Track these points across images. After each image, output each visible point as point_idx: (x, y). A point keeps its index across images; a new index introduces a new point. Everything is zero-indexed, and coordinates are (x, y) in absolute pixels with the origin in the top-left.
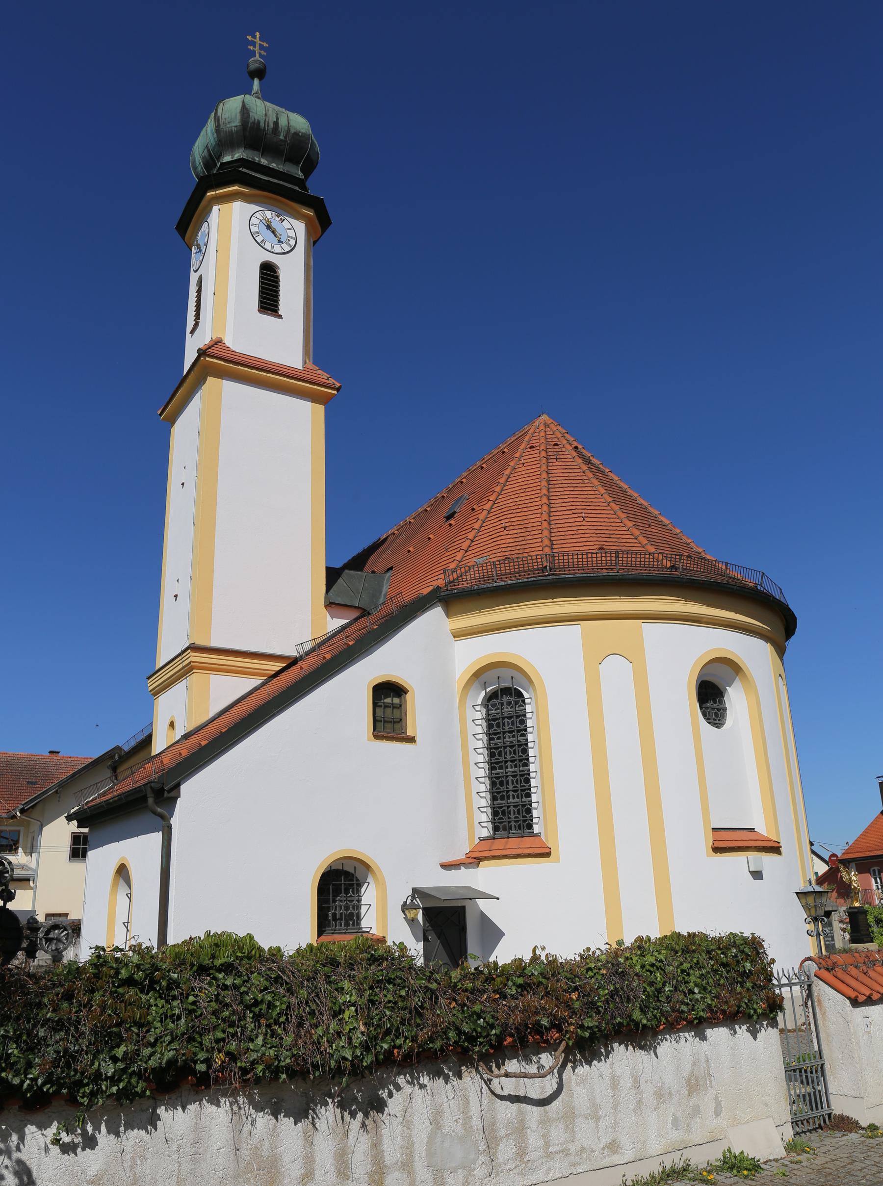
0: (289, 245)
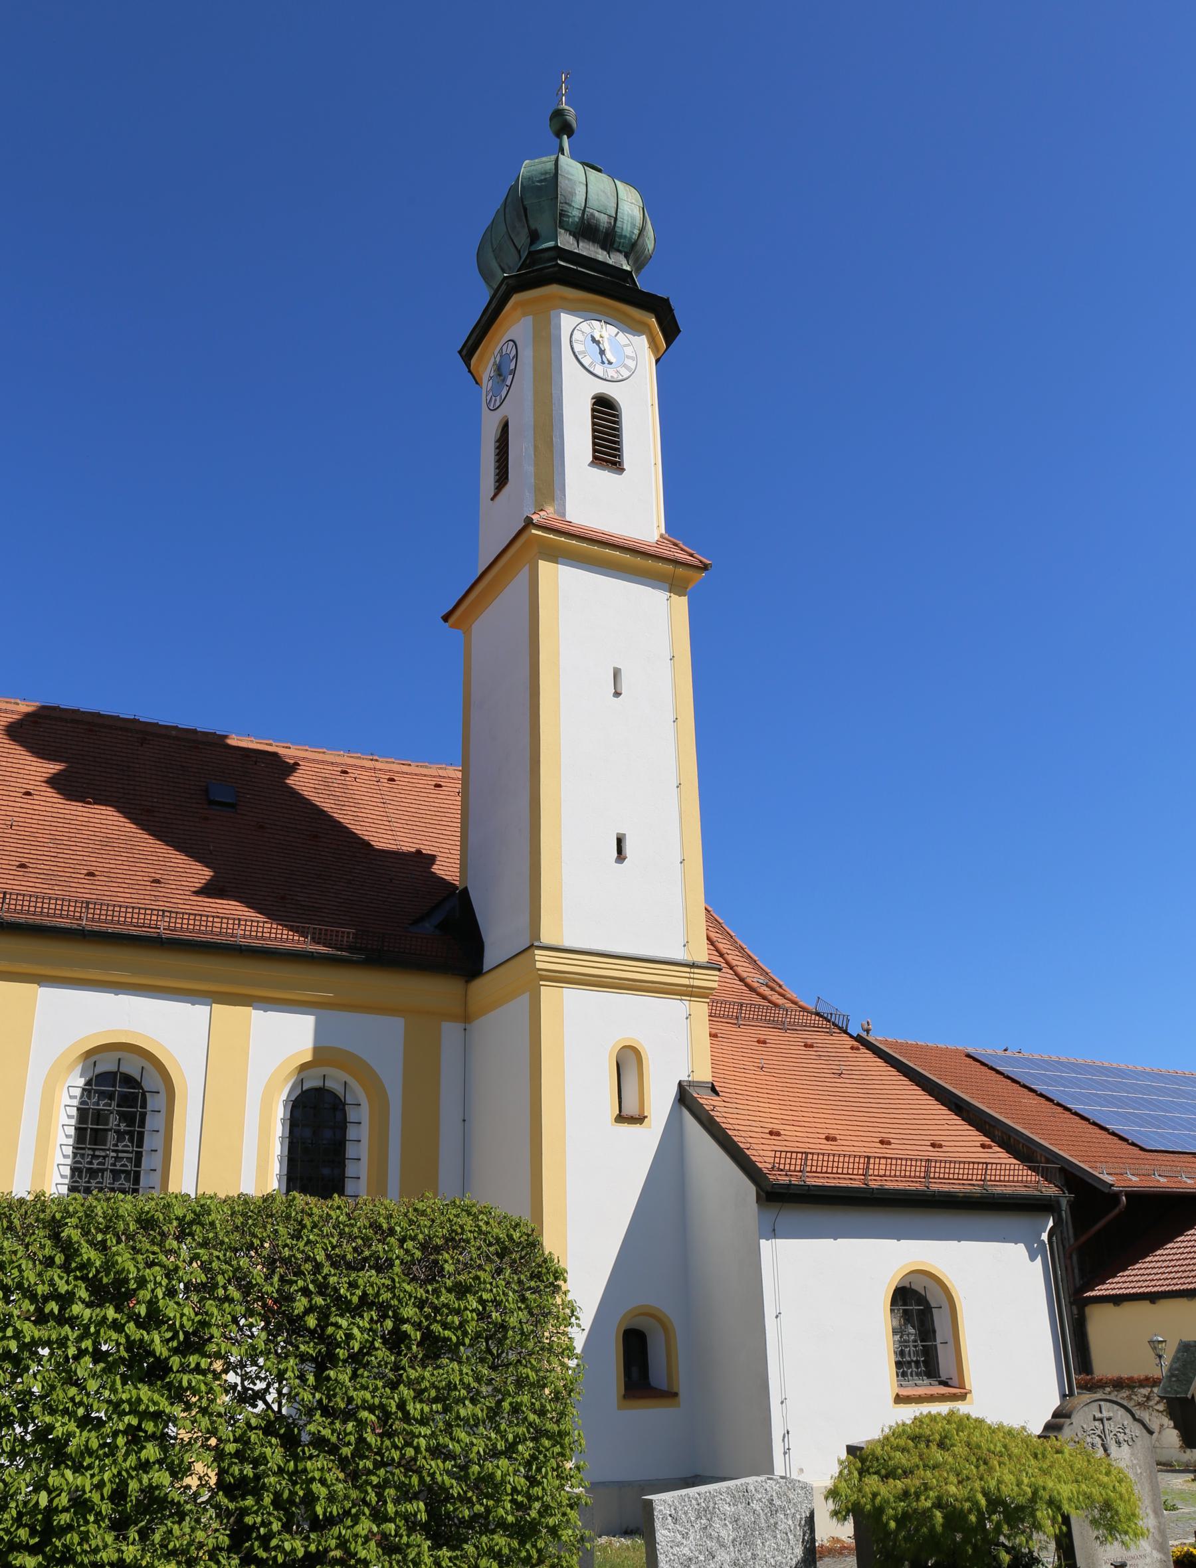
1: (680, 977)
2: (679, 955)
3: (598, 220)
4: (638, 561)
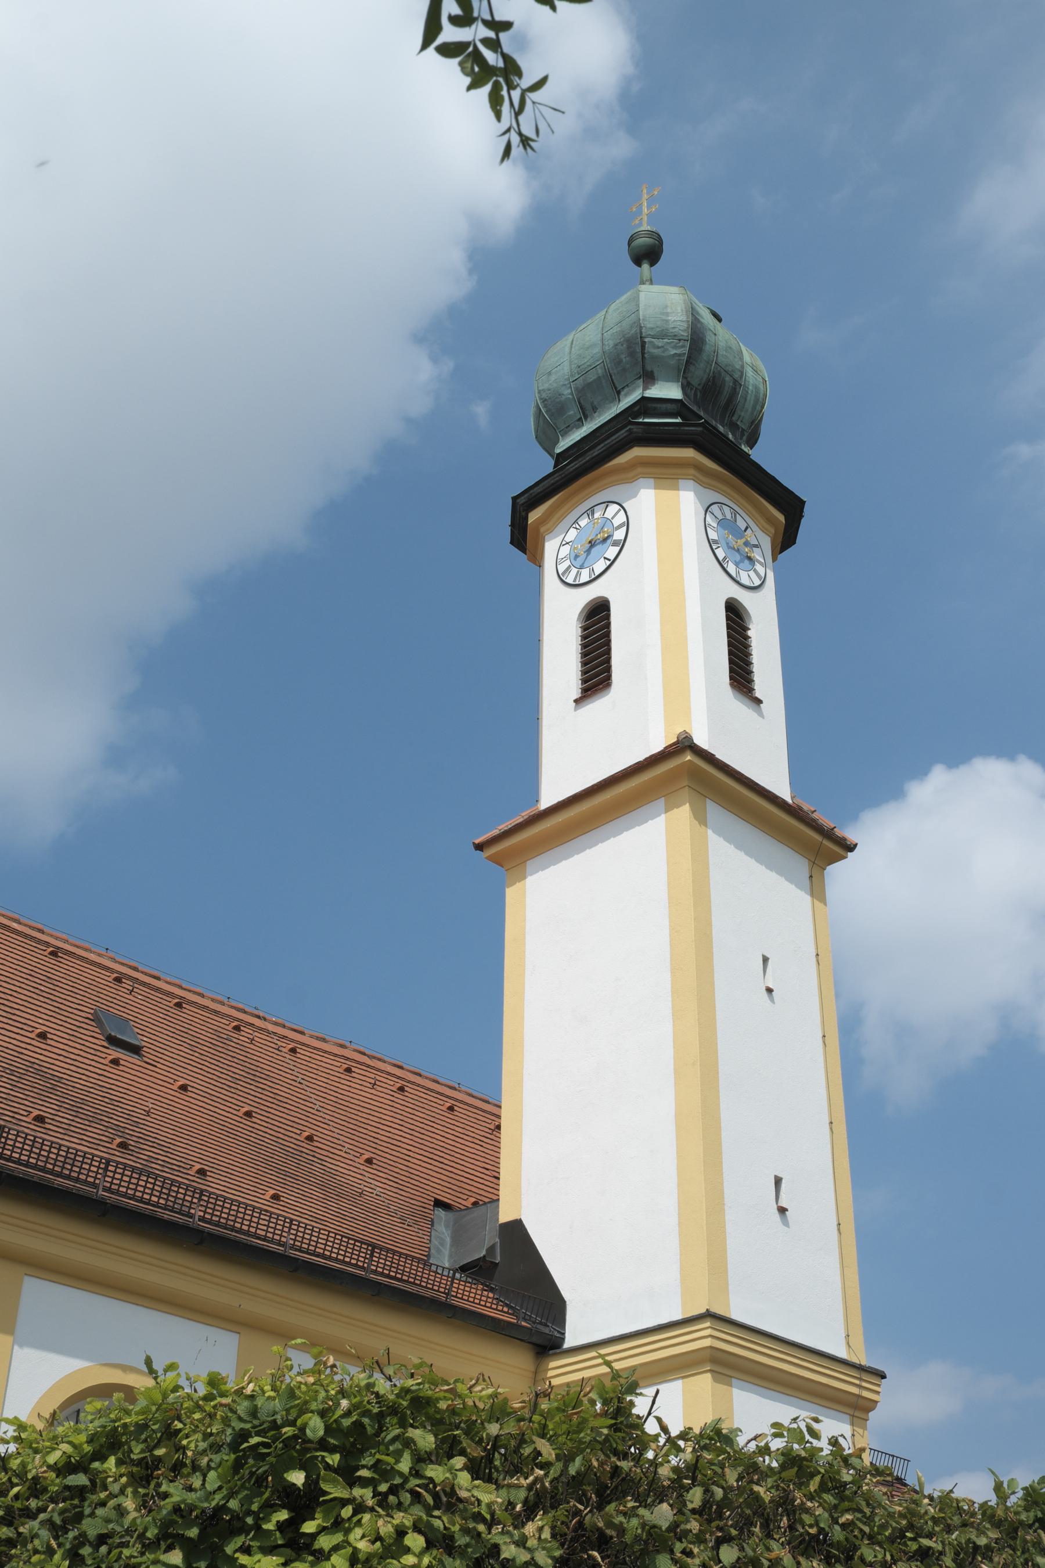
2: (842, 1353)
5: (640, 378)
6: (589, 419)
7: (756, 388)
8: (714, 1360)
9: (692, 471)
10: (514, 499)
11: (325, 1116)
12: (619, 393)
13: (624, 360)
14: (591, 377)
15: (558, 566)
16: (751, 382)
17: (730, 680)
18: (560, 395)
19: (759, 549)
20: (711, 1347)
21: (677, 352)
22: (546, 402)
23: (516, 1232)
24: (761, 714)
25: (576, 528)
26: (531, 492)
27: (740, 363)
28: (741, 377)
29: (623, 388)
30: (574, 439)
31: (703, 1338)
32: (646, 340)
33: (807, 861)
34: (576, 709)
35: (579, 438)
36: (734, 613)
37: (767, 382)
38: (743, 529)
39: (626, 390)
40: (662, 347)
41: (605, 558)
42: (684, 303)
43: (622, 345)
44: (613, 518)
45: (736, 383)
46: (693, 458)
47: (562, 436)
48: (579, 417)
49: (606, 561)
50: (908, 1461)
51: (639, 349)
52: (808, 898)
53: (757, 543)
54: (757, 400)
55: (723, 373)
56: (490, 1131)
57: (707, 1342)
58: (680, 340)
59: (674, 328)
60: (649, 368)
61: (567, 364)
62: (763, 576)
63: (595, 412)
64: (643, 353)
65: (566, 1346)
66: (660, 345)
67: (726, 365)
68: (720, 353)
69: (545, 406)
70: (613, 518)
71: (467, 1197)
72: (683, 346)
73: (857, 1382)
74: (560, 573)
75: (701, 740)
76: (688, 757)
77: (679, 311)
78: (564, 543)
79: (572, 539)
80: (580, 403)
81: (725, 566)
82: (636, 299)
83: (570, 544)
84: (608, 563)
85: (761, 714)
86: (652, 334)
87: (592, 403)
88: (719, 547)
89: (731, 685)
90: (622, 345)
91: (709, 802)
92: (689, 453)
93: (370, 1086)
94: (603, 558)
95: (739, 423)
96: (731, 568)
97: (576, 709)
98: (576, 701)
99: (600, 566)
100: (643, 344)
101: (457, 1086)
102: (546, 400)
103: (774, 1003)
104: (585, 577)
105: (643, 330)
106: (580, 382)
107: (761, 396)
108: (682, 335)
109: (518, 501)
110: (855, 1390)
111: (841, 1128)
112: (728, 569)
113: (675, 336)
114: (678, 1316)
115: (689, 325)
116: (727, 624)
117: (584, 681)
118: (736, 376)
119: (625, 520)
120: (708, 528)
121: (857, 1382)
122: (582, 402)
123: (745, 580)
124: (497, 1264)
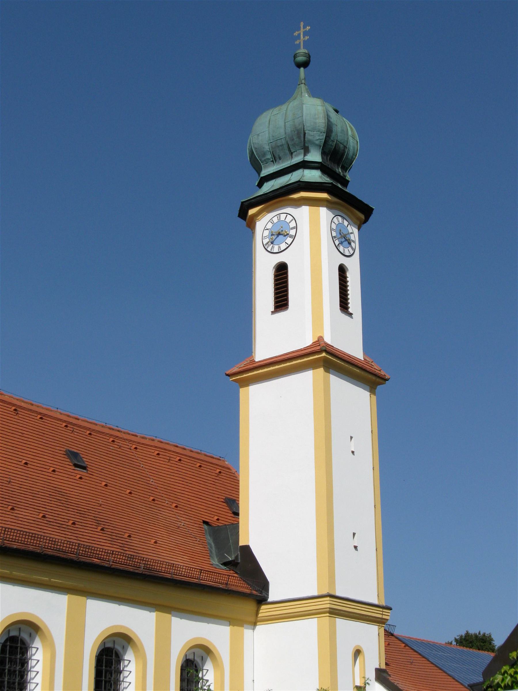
0: (291, 236)
1: (377, 613)
2: (376, 602)
3: (340, 148)
4: (363, 373)
5: (302, 149)
6: (277, 162)
7: (354, 148)
8: (330, 613)
9: (325, 203)
10: (242, 203)
11: (163, 495)
12: (292, 153)
13: (295, 139)
14: (279, 143)
15: (263, 240)
16: (352, 145)
17: (340, 307)
18: (263, 148)
19: (355, 244)
20: (330, 608)
21: (320, 138)
22: (256, 150)
23: (247, 550)
24: (352, 318)
25: (271, 222)
26: (251, 201)
27: (347, 137)
28: (347, 144)
29: (294, 152)
30: (269, 172)
31: (326, 603)
32: (306, 132)
33: (369, 387)
34: (272, 314)
35: (272, 172)
36: (342, 270)
37: (358, 142)
38: (346, 226)
39: (295, 153)
40: (313, 135)
41: (286, 243)
42: (324, 113)
43: (295, 132)
44: (290, 222)
45: (345, 147)
46: (327, 198)
47: (264, 169)
48: (272, 160)
49: (286, 244)
50: (395, 626)
51: (302, 135)
52: (369, 393)
53: (354, 240)
54: (353, 155)
55: (340, 144)
56: (216, 475)
57: (328, 606)
58: (321, 132)
59: (319, 126)
60: (307, 145)
61: (267, 132)
62: (354, 248)
63: (280, 160)
64: (304, 138)
65: (270, 600)
66: (312, 134)
67: (341, 140)
68: (339, 135)
69: (256, 151)
70: (290, 222)
71: (214, 516)
72: (322, 136)
73: (381, 613)
74: (264, 244)
75: (328, 339)
76: (324, 354)
77: (321, 117)
78: (266, 229)
79: (270, 228)
80: (273, 154)
81: (339, 248)
82: (301, 107)
83: (269, 230)
84: (287, 246)
85: (352, 318)
86: (309, 129)
87: (279, 155)
88: (336, 239)
89: (340, 309)
90: (295, 132)
91: (331, 370)
92: (325, 195)
93: (167, 461)
94: (284, 242)
95: (345, 165)
96: (341, 248)
97: (272, 314)
98: (272, 312)
99: (283, 246)
100: (305, 134)
101: (200, 451)
102: (256, 148)
103: (351, 440)
104: (276, 250)
105: (305, 127)
106: (273, 144)
107: (355, 153)
108: (322, 130)
109: (244, 203)
110: (380, 616)
111: (379, 506)
112: (340, 250)
113: (319, 130)
114: (316, 594)
115: (326, 125)
116: (339, 278)
117: (276, 303)
118: (345, 144)
119: (295, 225)
120: (332, 231)
121: (381, 613)
122: (274, 153)
123: (347, 253)
124: (238, 563)
